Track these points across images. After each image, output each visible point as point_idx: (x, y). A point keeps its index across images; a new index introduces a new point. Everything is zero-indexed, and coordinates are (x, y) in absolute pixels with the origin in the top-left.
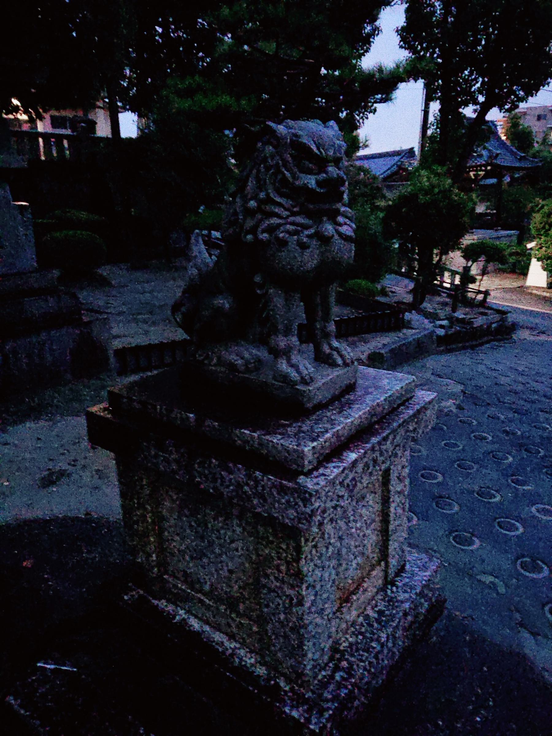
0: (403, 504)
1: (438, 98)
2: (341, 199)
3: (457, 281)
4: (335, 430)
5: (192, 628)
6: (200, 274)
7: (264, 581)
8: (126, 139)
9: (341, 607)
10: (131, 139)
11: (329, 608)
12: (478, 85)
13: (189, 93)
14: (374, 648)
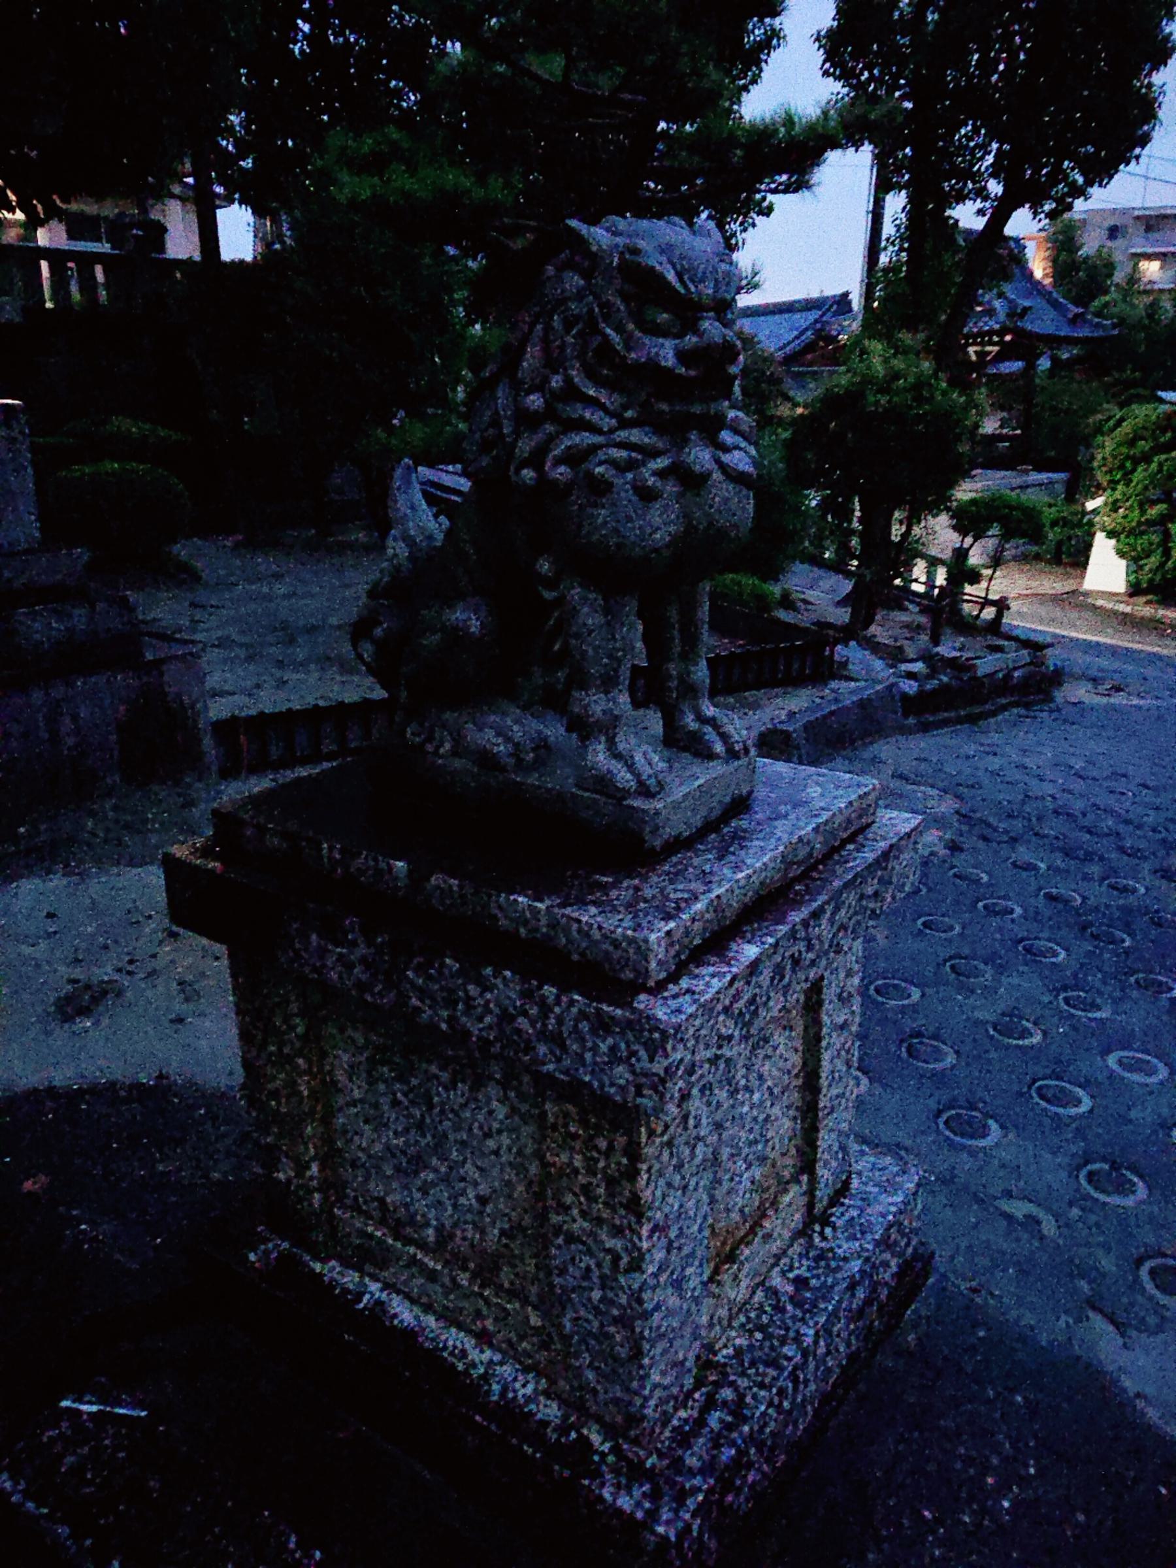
0: (848, 1052)
1: (906, 186)
2: (728, 395)
3: (941, 578)
4: (713, 895)
5: (396, 1322)
6: (412, 558)
7: (555, 1219)
8: (233, 262)
9: (716, 1271)
10: (242, 262)
11: (694, 1277)
12: (990, 159)
13: (375, 164)
14: (789, 1359)
